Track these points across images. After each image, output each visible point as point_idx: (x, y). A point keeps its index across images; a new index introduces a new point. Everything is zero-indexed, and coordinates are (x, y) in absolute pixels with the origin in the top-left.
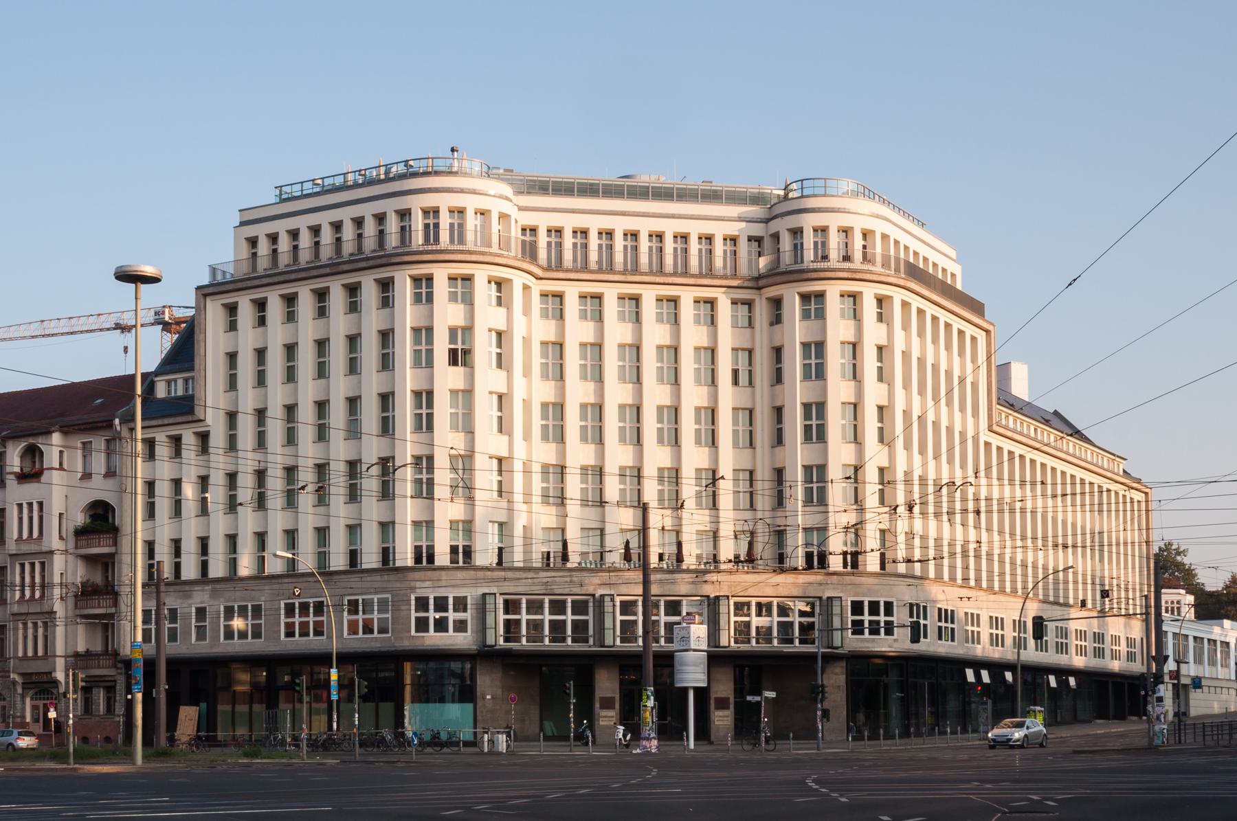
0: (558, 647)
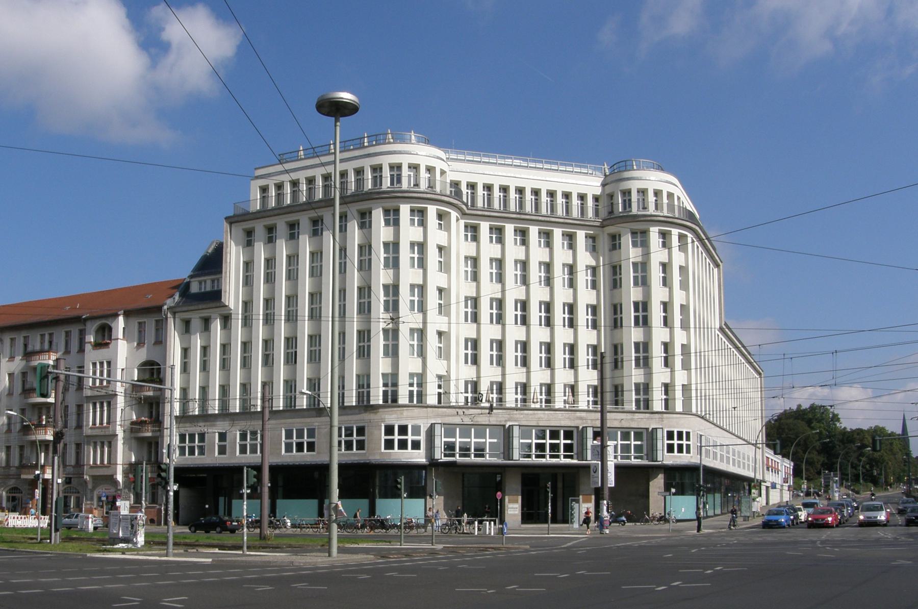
0: (479, 460)
